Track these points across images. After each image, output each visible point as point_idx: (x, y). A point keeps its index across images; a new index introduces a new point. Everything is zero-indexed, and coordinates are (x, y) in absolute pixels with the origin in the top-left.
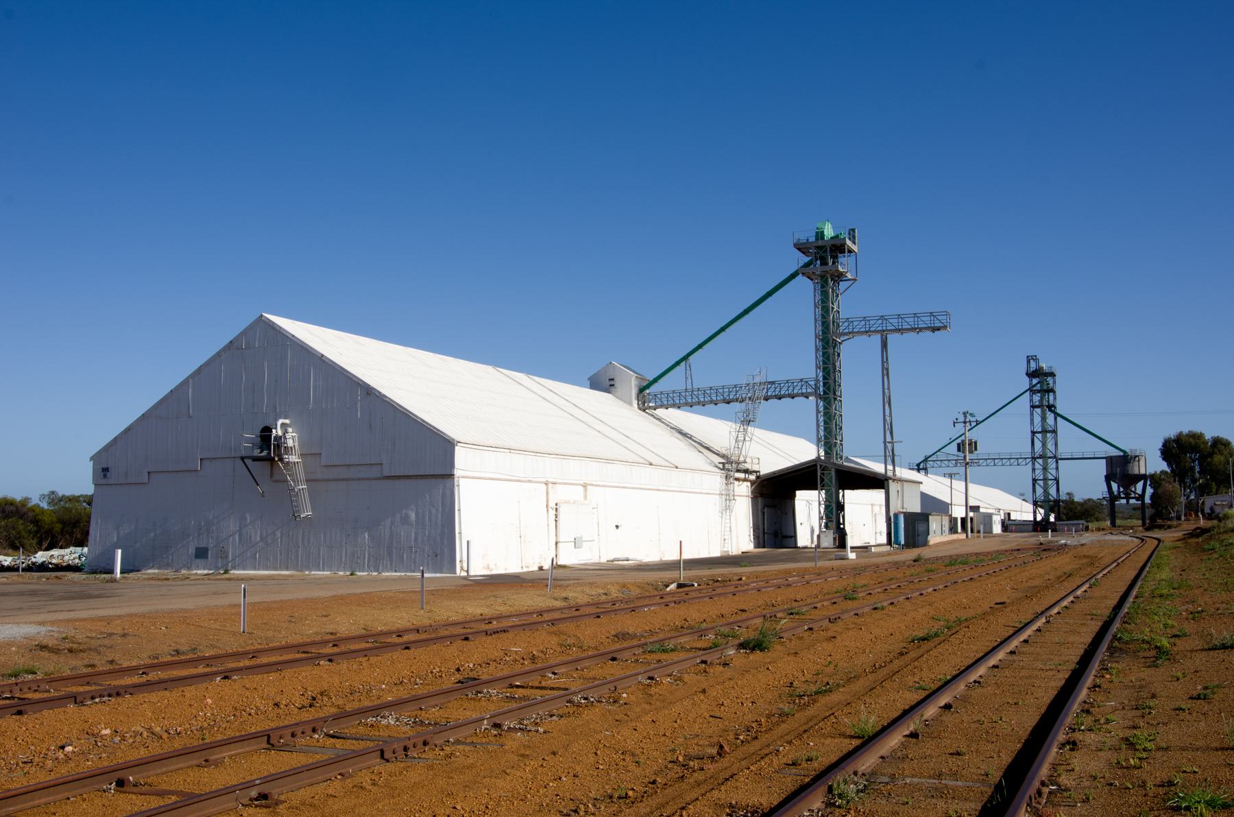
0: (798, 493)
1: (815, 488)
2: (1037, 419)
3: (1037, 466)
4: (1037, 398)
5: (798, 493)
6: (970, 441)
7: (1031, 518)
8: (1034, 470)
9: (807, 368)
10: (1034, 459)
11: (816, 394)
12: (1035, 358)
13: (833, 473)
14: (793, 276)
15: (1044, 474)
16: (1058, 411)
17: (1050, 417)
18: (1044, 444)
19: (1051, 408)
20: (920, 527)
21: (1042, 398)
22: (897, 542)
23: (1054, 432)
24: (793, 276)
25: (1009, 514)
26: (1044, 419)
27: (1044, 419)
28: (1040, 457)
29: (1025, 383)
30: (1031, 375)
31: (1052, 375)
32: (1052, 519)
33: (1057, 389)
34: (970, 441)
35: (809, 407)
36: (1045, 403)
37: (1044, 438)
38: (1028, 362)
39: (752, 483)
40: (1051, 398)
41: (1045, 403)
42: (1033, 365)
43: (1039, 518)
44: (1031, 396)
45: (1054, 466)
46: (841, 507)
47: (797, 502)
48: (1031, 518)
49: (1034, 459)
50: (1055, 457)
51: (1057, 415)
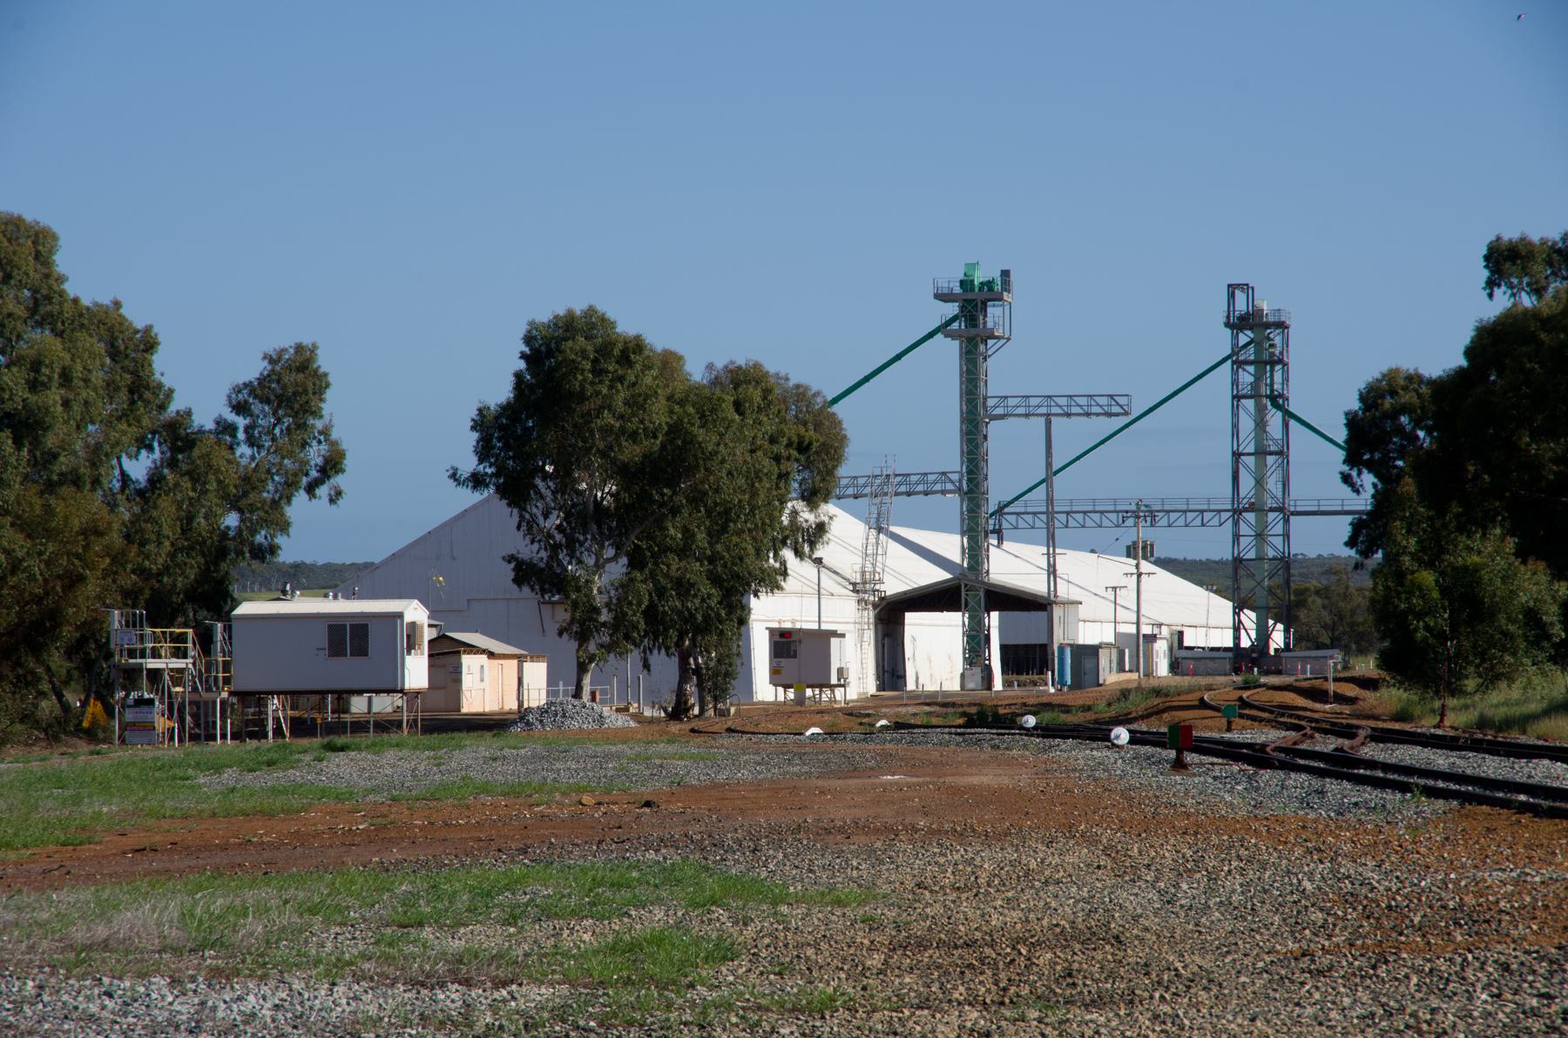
0: (908, 615)
1: (957, 609)
2: (1247, 424)
3: (1244, 529)
4: (1246, 377)
5: (908, 615)
6: (1145, 542)
7: (1230, 644)
8: (1236, 537)
9: (951, 459)
10: (1237, 513)
11: (960, 489)
12: (1245, 287)
13: (982, 595)
14: (931, 335)
15: (1259, 548)
16: (1292, 409)
17: (1275, 419)
18: (1260, 482)
19: (1278, 400)
20: (1088, 664)
21: (1258, 378)
22: (1063, 684)
23: (1282, 453)
24: (931, 335)
25: (1181, 634)
26: (1261, 424)
27: (1261, 424)
28: (1252, 508)
29: (1223, 342)
30: (1238, 323)
31: (1282, 326)
32: (1278, 639)
33: (1292, 358)
34: (1145, 542)
35: (953, 504)
36: (1265, 390)
37: (1261, 465)
38: (1231, 296)
39: (875, 606)
40: (1278, 377)
41: (1265, 390)
42: (1241, 305)
43: (1245, 643)
44: (1235, 373)
45: (1279, 529)
46: (298, 567)
47: (909, 632)
48: (1230, 644)
49: (1237, 513)
50: (1281, 509)
51: (1288, 415)
